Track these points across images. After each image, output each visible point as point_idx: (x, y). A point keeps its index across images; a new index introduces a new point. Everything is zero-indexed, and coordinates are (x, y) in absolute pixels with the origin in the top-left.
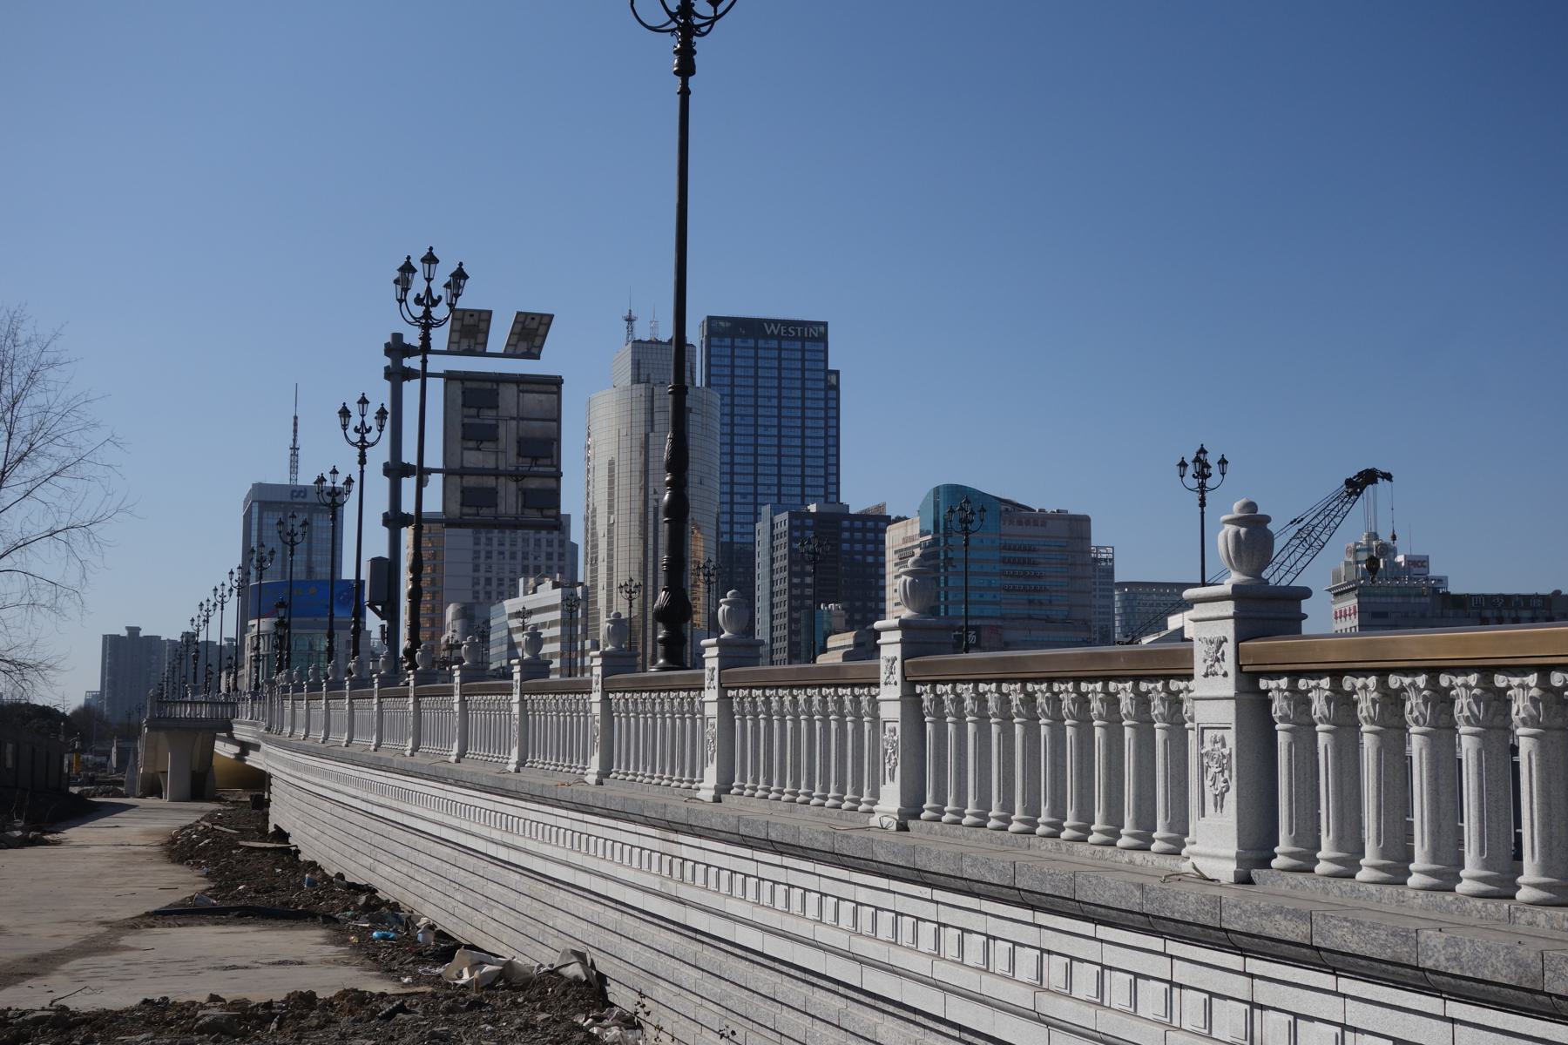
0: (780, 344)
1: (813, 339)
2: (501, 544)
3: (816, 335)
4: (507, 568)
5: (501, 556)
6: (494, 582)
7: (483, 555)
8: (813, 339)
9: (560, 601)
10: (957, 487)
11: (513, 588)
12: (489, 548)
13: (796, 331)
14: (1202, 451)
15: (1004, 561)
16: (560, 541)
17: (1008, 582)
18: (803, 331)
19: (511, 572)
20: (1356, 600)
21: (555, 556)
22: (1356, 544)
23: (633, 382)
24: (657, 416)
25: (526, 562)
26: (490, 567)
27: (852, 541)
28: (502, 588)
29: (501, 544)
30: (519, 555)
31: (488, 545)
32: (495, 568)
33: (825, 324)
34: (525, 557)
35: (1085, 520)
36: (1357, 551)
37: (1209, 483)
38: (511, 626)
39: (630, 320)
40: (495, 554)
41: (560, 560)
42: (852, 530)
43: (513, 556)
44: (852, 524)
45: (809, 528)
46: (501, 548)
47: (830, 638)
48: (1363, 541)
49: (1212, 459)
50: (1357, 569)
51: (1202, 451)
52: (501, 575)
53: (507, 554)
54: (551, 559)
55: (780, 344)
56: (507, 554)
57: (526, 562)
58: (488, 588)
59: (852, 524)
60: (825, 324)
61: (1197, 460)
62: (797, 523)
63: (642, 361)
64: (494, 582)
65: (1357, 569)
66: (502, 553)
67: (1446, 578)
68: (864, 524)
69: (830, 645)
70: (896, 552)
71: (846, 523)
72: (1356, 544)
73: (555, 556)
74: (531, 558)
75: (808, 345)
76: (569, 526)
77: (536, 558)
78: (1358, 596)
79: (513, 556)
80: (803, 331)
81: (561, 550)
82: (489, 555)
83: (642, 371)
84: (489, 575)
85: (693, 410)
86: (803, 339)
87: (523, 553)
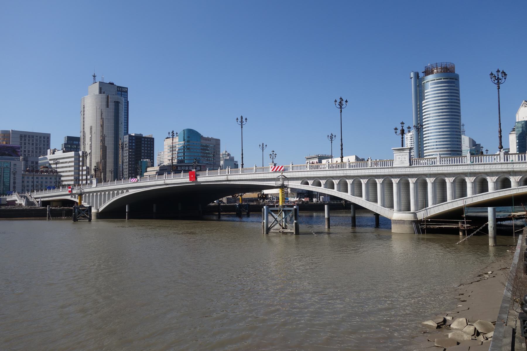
0: (121, 93)
1: (124, 92)
2: (29, 141)
3: (125, 91)
4: (31, 148)
5: (29, 144)
6: (27, 151)
7: (23, 144)
8: (124, 92)
9: (74, 155)
10: (191, 129)
11: (33, 153)
12: (25, 142)
13: (120, 89)
14: (173, 131)
15: (201, 149)
16: (47, 141)
17: (452, 139)
18: (121, 89)
19: (32, 149)
20: (318, 160)
21: (46, 145)
22: (223, 153)
23: (99, 93)
24: (109, 103)
25: (37, 146)
26: (25, 147)
27: (144, 144)
28: (29, 153)
29: (29, 141)
30: (35, 144)
31: (24, 141)
32: (27, 148)
33: (127, 88)
34: (37, 145)
35: (219, 140)
36: (223, 155)
37: (333, 139)
38: (50, 163)
39: (94, 76)
40: (27, 144)
41: (47, 146)
42: (145, 141)
43: (33, 144)
44: (148, 140)
45: (134, 140)
46: (29, 142)
47: (148, 168)
48: (224, 152)
49: (175, 133)
50: (223, 159)
51: (173, 131)
52: (29, 150)
53: (31, 144)
54: (45, 146)
55: (121, 93)
56: (31, 144)
57: (37, 146)
58: (25, 153)
59: (148, 140)
60: (127, 88)
61: (172, 132)
62: (131, 138)
63: (102, 88)
64: (27, 151)
65: (223, 159)
66: (29, 143)
67: (237, 161)
68: (144, 139)
69: (148, 170)
70: (168, 146)
71: (143, 139)
72: (223, 153)
73: (46, 145)
74: (38, 145)
75: (123, 93)
76: (50, 137)
77: (40, 145)
78: (318, 159)
79: (33, 144)
80: (121, 89)
81: (48, 144)
82: (25, 144)
83: (102, 90)
84: (25, 149)
85: (120, 103)
86: (121, 91)
87: (36, 144)
